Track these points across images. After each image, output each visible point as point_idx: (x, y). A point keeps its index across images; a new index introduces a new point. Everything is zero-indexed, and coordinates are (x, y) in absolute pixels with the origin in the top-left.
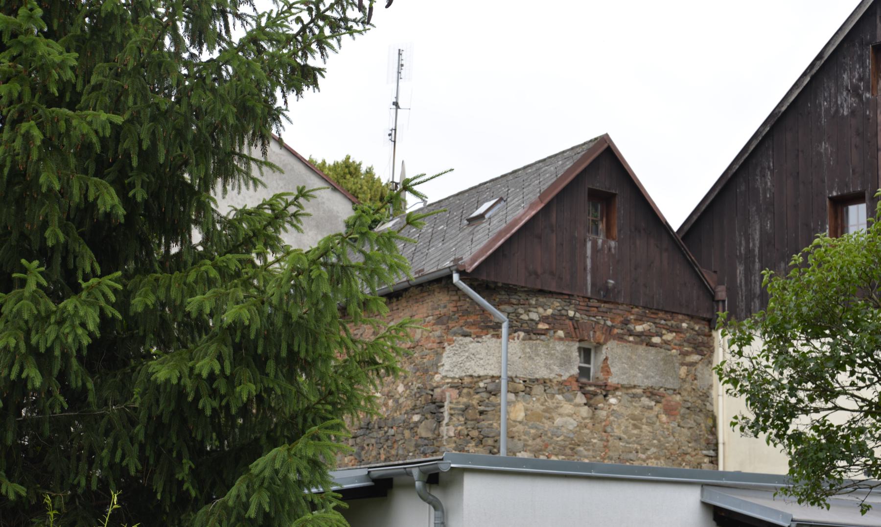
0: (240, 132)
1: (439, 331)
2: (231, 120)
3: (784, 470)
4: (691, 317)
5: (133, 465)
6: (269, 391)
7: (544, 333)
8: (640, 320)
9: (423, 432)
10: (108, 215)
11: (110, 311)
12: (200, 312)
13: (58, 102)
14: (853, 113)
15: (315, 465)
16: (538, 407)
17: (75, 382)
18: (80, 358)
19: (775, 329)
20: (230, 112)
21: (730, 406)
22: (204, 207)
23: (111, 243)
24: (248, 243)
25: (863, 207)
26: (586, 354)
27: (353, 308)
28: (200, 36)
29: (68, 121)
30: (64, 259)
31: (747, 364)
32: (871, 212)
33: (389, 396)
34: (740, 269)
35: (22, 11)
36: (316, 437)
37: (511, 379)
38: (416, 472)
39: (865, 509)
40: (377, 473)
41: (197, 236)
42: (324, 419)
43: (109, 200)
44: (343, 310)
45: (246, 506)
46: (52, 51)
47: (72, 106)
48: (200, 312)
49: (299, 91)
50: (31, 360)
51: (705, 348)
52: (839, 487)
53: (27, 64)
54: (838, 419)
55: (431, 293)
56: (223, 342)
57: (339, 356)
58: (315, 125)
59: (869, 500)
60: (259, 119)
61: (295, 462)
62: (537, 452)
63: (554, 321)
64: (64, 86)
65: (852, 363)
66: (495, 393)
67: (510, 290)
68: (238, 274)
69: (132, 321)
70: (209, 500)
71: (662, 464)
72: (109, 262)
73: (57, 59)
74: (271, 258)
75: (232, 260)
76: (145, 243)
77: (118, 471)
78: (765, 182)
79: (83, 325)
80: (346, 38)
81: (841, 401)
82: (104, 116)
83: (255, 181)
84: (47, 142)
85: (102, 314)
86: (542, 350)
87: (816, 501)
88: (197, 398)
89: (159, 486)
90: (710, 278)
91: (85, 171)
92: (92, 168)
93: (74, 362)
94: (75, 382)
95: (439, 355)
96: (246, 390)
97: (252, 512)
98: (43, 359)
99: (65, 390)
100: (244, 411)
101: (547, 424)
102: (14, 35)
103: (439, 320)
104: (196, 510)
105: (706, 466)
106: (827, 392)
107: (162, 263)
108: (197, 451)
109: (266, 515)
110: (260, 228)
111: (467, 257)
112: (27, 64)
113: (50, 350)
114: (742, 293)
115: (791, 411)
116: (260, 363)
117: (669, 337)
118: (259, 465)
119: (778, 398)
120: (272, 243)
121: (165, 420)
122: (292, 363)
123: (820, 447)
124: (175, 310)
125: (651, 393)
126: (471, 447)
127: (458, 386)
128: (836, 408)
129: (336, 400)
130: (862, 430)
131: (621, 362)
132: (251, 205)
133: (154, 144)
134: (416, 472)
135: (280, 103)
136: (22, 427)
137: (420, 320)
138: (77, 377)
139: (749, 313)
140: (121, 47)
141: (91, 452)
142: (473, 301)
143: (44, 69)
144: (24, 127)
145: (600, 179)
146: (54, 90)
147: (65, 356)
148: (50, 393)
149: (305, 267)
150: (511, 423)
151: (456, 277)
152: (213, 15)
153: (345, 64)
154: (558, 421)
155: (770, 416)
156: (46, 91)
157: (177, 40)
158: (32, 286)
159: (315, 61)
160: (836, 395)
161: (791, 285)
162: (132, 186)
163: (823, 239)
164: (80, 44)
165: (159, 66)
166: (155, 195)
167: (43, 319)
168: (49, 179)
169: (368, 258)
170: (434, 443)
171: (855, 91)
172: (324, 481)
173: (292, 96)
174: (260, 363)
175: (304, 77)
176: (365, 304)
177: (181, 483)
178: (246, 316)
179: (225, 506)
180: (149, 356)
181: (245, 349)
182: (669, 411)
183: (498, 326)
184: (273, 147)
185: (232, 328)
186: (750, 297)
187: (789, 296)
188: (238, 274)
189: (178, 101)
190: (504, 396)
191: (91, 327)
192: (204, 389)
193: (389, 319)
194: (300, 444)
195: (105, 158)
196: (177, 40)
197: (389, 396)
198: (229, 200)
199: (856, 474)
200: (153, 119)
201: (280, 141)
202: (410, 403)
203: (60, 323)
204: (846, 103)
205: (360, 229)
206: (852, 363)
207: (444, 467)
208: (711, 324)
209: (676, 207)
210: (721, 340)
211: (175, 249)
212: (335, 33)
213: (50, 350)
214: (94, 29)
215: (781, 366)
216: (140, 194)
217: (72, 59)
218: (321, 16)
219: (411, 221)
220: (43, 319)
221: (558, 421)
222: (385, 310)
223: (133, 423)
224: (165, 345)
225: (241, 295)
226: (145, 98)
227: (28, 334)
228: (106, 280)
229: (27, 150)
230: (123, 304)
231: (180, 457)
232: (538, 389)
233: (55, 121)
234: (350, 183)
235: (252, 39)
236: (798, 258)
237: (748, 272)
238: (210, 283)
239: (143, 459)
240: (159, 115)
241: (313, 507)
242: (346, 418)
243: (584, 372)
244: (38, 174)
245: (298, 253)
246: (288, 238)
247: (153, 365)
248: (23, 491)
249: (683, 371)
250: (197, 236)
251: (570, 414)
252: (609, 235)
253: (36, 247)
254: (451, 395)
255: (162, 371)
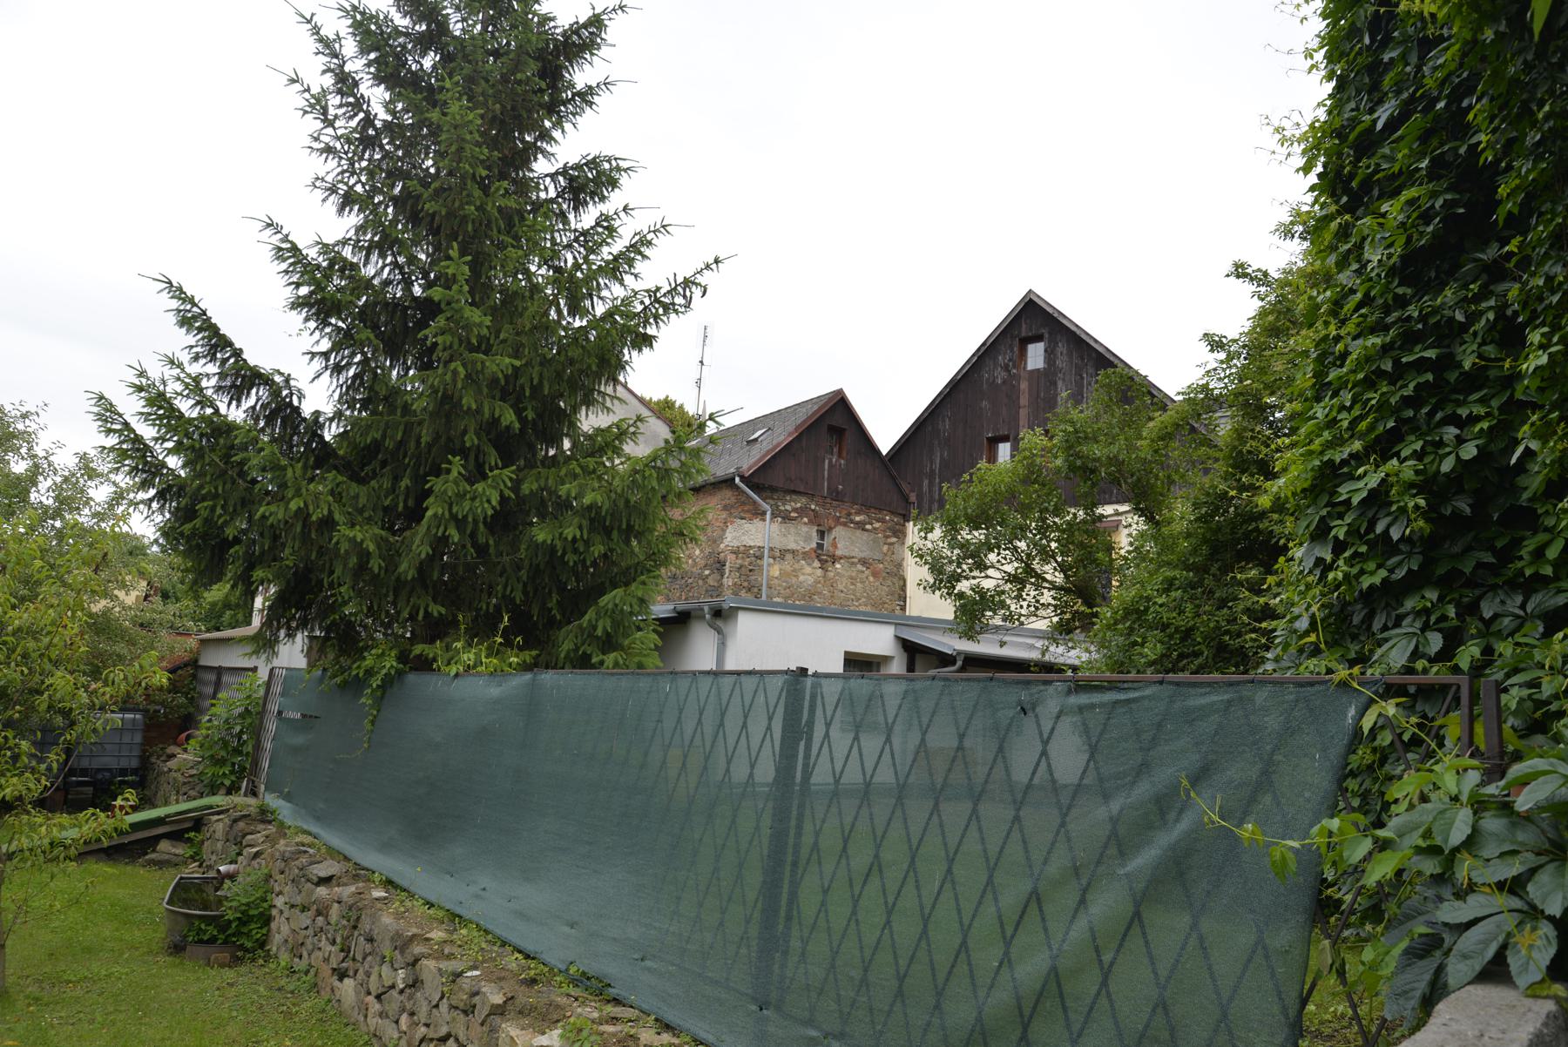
0: (598, 376)
1: (724, 515)
2: (594, 368)
3: (951, 617)
4: (892, 513)
5: (518, 597)
6: (612, 550)
7: (794, 519)
8: (858, 513)
9: (711, 581)
10: (508, 428)
11: (507, 493)
12: (568, 495)
13: (477, 350)
14: (1004, 382)
15: (642, 601)
16: (788, 568)
17: (482, 540)
18: (485, 523)
19: (949, 523)
20: (594, 363)
21: (915, 572)
22: (573, 425)
23: (510, 447)
24: (601, 451)
25: (1008, 445)
26: (822, 534)
27: (671, 497)
28: (575, 310)
29: (483, 363)
30: (477, 457)
31: (930, 545)
32: (1015, 448)
33: (690, 557)
34: (926, 482)
35: (455, 287)
36: (644, 583)
37: (771, 549)
38: (706, 609)
39: (1002, 644)
40: (680, 608)
41: (567, 444)
42: (649, 571)
43: (509, 417)
44: (664, 497)
45: (595, 628)
46: (475, 315)
47: (486, 353)
48: (568, 495)
49: (640, 350)
50: (452, 524)
51: (900, 534)
52: (986, 628)
53: (457, 323)
54: (988, 584)
55: (720, 489)
56: (583, 516)
57: (660, 529)
58: (649, 374)
59: (1006, 639)
60: (611, 366)
61: (629, 599)
62: (786, 598)
63: (802, 512)
64: (481, 338)
65: (999, 548)
66: (760, 558)
67: (773, 489)
68: (594, 471)
69: (521, 500)
70: (569, 622)
71: (869, 609)
72: (507, 459)
73: (477, 320)
74: (617, 461)
75: (591, 462)
76: (532, 449)
77: (508, 600)
78: (945, 425)
79: (489, 501)
80: (673, 316)
81: (991, 572)
82: (507, 360)
83: (608, 409)
84: (468, 376)
85: (502, 495)
86: (792, 530)
87: (970, 638)
88: (564, 553)
89: (535, 612)
90: (905, 487)
91: (493, 398)
92: (498, 395)
93: (481, 526)
94: (482, 540)
95: (724, 531)
96: (598, 549)
97: (599, 632)
98: (460, 523)
99: (475, 545)
100: (594, 564)
101: (794, 580)
102: (449, 303)
103: (725, 508)
104: (559, 628)
105: (898, 612)
106: (982, 566)
107: (543, 462)
108: (562, 589)
109: (608, 634)
110: (608, 442)
111: (745, 467)
112: (457, 323)
113: (465, 517)
114: (926, 499)
115: (957, 578)
116: (608, 532)
117: (877, 525)
118: (605, 600)
119: (950, 568)
120: (618, 451)
121: (542, 567)
122: (629, 532)
123: (975, 602)
124: (550, 493)
125: (864, 562)
126: (743, 593)
127: (736, 552)
128: (987, 577)
129: (658, 558)
130: (1003, 592)
131: (845, 541)
132: (604, 425)
133: (541, 382)
134: (706, 609)
135: (627, 357)
136: (444, 567)
137: (713, 507)
138: (483, 536)
139: (930, 513)
140: (521, 315)
141: (490, 587)
142: (748, 496)
143: (468, 327)
144: (453, 365)
145: (834, 419)
146: (474, 341)
147: (475, 521)
148: (464, 546)
149: (639, 471)
150: (770, 578)
151: (737, 480)
152: (583, 297)
153: (671, 333)
154: (802, 578)
155: (944, 580)
156: (469, 343)
157: (559, 312)
158: (455, 473)
159: (651, 331)
160: (987, 568)
161: (961, 494)
162: (525, 409)
163: (983, 464)
164: (494, 311)
165: (548, 328)
166: (540, 416)
167: (461, 496)
168: (468, 401)
169: (683, 464)
170: (718, 589)
171: (1006, 368)
172: (648, 613)
173: (635, 353)
174: (608, 532)
175: (646, 341)
176: (679, 495)
177: (550, 610)
178: (599, 500)
179: (580, 627)
180: (532, 524)
181: (598, 522)
182: (875, 574)
183: (764, 513)
184: (619, 388)
185: (589, 508)
186: (931, 502)
187: (959, 501)
188: (594, 471)
189: (558, 353)
190: (766, 560)
191: (494, 503)
192: (569, 549)
193: (693, 506)
194: (633, 586)
195: (507, 389)
196: (559, 312)
197: (690, 557)
198: (590, 421)
199: (997, 621)
200: (541, 364)
201: (625, 386)
202: (703, 562)
203: (473, 499)
204: (1000, 376)
205: (675, 446)
206: (999, 548)
207: (725, 606)
208: (906, 518)
209: (885, 437)
210: (913, 532)
211: (552, 452)
212: (666, 312)
213: (465, 517)
214: (503, 302)
215: (952, 548)
216: (530, 415)
217: (487, 321)
218: (657, 301)
219: (712, 440)
220: (461, 496)
221: (802, 578)
222: (693, 499)
223: (519, 568)
224: (542, 516)
225: (597, 485)
226: (536, 350)
227: (451, 505)
228: (506, 472)
229: (454, 381)
230: (516, 488)
231: (550, 593)
232: (789, 556)
233: (474, 363)
234: (668, 413)
235: (609, 314)
236: (966, 477)
237: (931, 484)
238: (575, 476)
239: (525, 593)
240: (545, 362)
241: (639, 629)
242: (663, 570)
243: (820, 546)
244: (461, 399)
245: (638, 460)
246: (628, 448)
247: (535, 530)
248: (443, 611)
249: (885, 548)
250: (567, 444)
251: (809, 573)
252: (840, 456)
253: (458, 447)
254: (731, 558)
255: (541, 535)
